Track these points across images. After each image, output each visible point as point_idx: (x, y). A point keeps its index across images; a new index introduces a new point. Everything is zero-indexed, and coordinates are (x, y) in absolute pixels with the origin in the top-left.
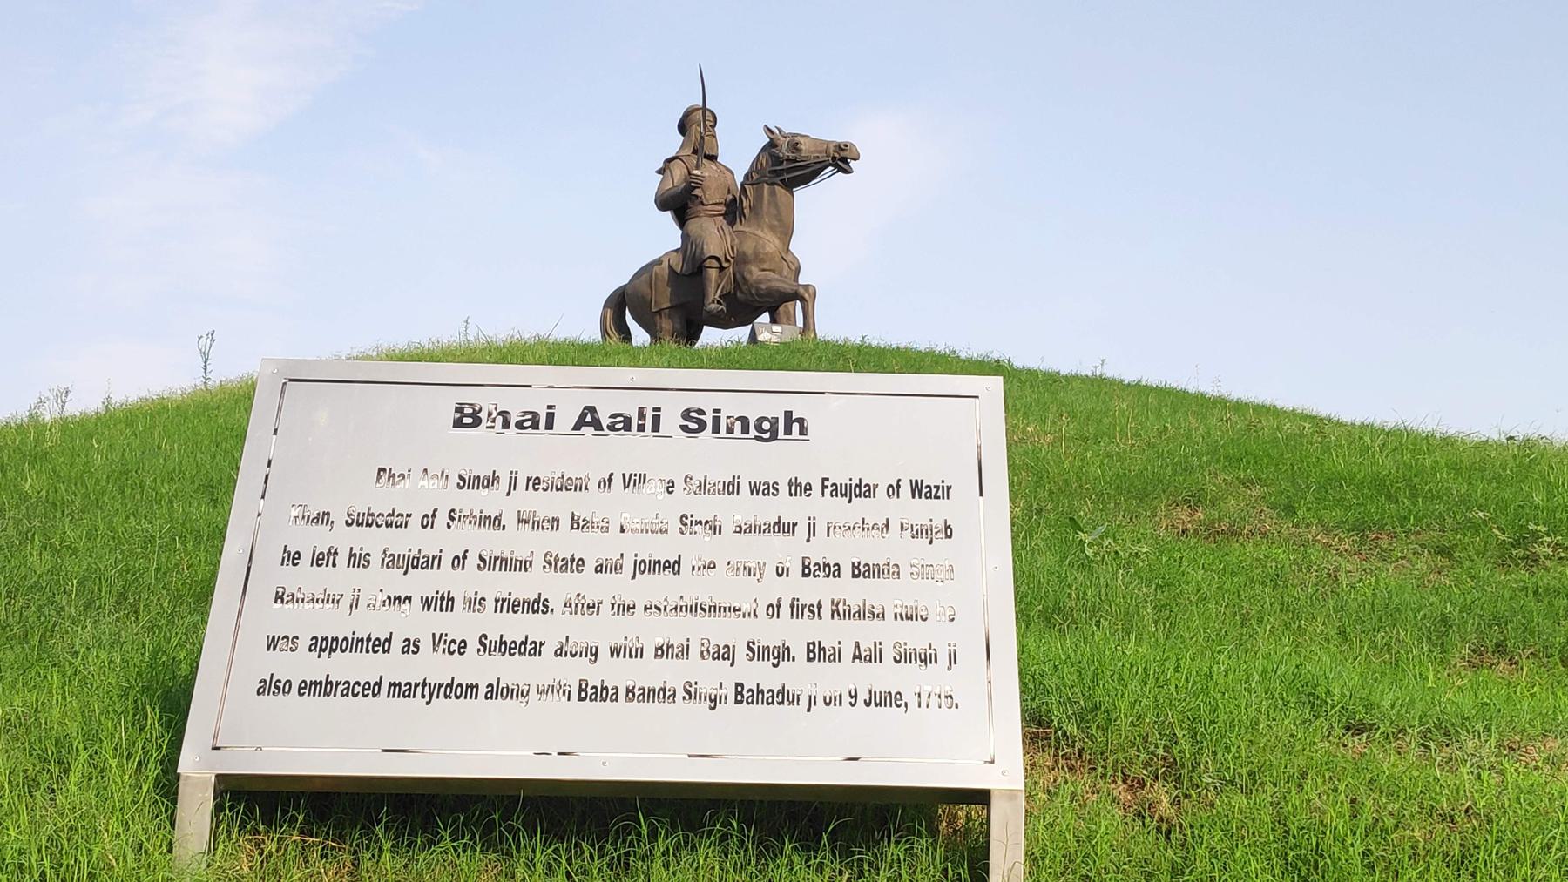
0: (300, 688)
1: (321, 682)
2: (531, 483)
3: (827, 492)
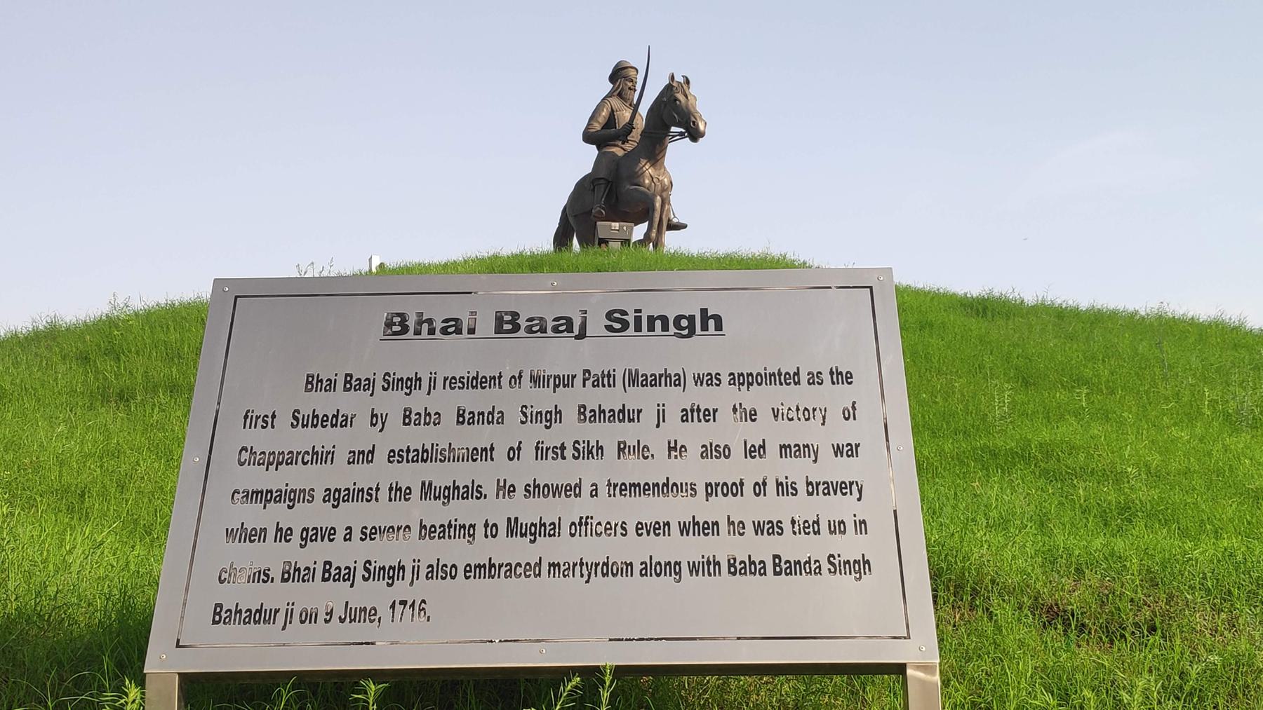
0: (466, 571)
1: (485, 565)
2: (448, 382)
3: (589, 383)
